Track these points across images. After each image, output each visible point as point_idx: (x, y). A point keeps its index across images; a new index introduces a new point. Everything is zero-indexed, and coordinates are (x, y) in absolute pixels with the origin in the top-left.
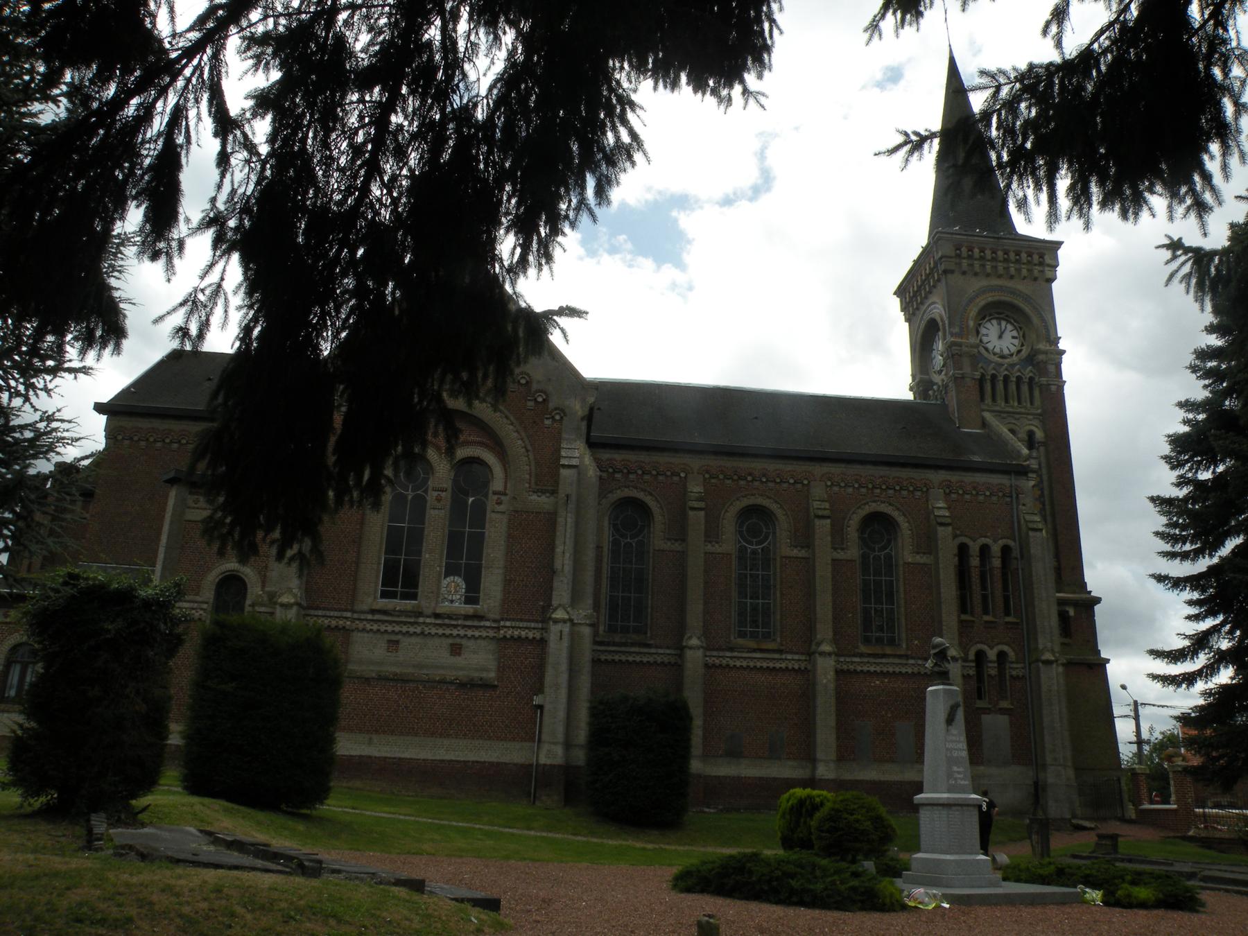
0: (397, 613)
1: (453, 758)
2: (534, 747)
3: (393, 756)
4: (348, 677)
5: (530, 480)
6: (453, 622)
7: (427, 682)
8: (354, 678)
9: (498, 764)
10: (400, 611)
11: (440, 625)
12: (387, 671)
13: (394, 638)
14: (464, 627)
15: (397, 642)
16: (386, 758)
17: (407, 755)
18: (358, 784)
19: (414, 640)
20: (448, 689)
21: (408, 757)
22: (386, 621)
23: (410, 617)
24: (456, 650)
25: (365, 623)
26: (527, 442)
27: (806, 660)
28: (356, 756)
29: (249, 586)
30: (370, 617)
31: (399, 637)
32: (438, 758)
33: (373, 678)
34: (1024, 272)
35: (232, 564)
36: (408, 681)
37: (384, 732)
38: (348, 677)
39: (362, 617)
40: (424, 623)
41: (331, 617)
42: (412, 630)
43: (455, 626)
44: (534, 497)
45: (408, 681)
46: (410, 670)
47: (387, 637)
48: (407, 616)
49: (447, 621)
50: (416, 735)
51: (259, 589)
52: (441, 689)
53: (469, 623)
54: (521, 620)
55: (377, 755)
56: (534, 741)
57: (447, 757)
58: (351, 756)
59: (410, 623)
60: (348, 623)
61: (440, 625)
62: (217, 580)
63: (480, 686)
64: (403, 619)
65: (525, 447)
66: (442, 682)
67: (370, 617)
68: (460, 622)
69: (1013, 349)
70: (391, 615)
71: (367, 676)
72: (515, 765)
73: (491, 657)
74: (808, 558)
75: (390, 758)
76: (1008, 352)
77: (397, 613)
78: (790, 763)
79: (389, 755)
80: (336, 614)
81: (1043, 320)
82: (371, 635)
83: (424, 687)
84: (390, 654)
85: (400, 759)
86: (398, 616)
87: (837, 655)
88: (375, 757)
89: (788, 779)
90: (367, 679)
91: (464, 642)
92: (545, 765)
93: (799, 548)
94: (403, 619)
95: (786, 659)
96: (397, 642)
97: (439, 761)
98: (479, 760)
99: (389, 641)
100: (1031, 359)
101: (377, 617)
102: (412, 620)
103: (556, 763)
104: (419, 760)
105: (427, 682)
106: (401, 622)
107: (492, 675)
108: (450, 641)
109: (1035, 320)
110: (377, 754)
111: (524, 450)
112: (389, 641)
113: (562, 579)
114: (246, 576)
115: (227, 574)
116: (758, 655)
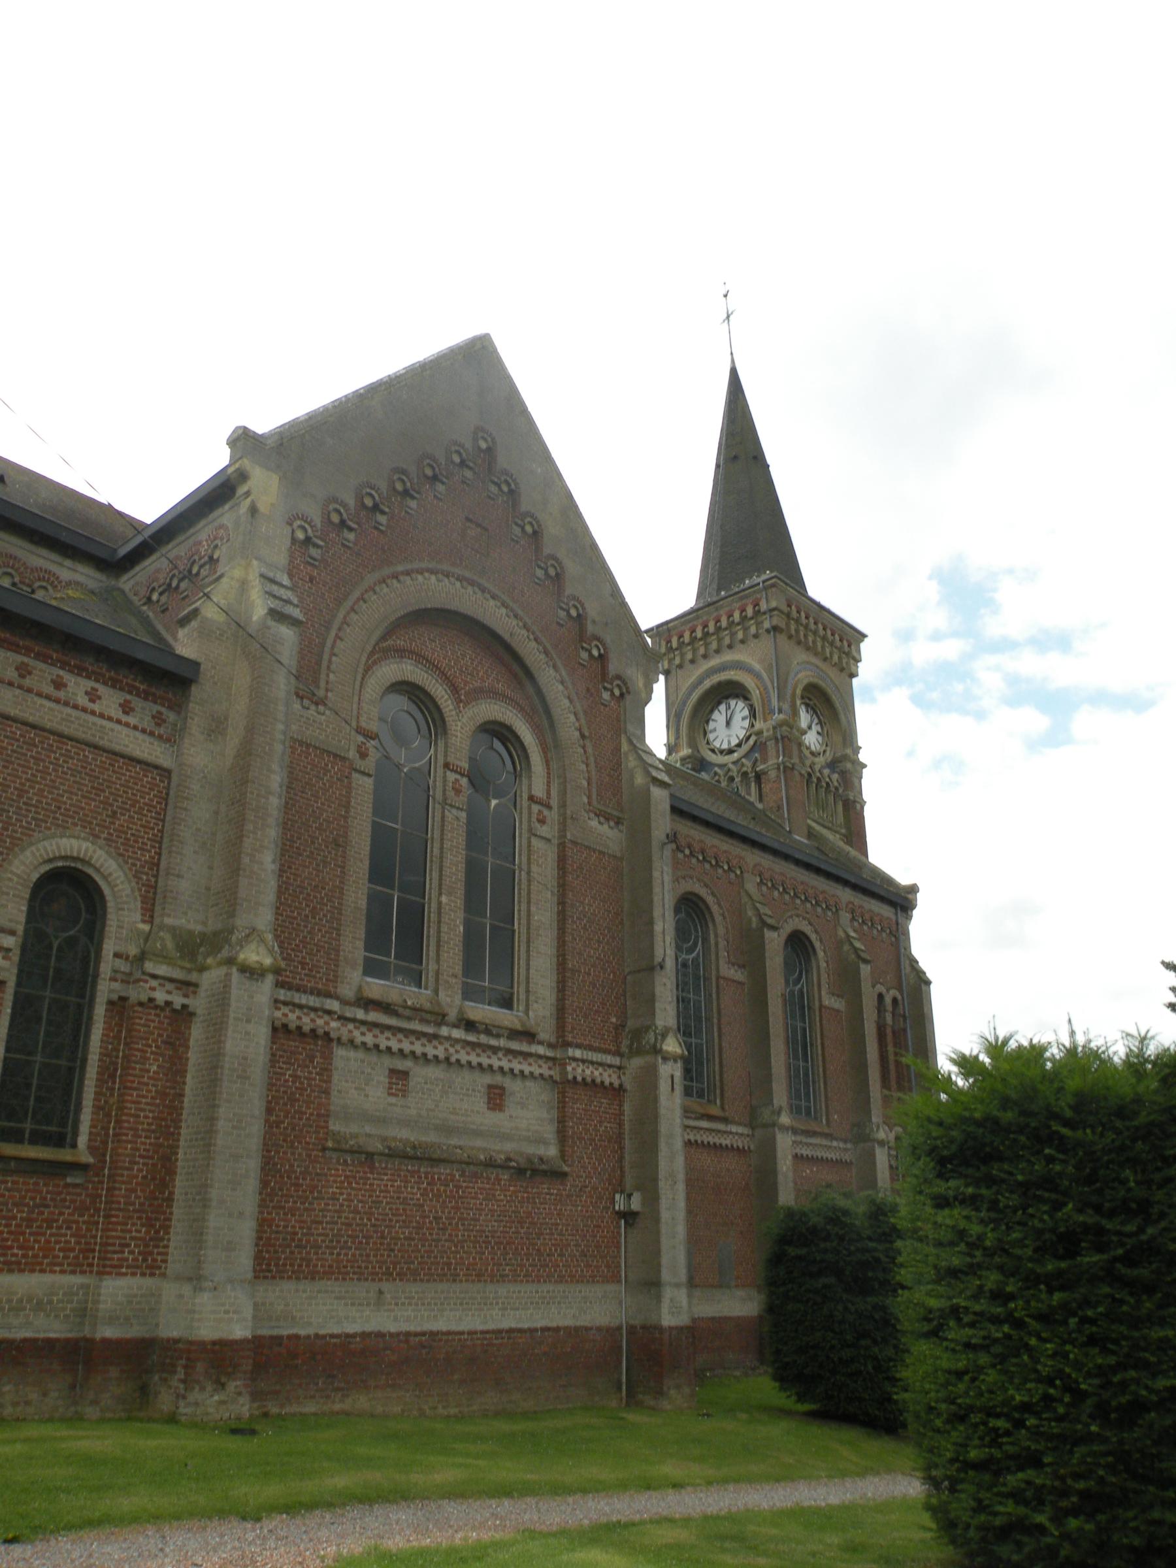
0: (407, 1013)
1: (513, 1325)
2: (620, 1292)
3: (419, 1329)
4: (335, 1150)
5: (590, 791)
6: (493, 1042)
7: (468, 1164)
8: (346, 1151)
9: (577, 1329)
10: (415, 1009)
11: (474, 1045)
12: (395, 1139)
13: (402, 1065)
14: (509, 1052)
15: (405, 1075)
16: (408, 1334)
17: (440, 1325)
18: (361, 1401)
19: (433, 1072)
20: (498, 1180)
21: (444, 1329)
22: (389, 1028)
23: (428, 1022)
24: (496, 1098)
25: (351, 1026)
26: (583, 721)
27: (748, 1136)
28: (354, 1336)
29: (111, 904)
30: (360, 1014)
31: (407, 1064)
32: (491, 1326)
33: (381, 1154)
34: (836, 658)
35: (74, 842)
36: (436, 1161)
37: (401, 1276)
38: (335, 1150)
39: (348, 1015)
40: (448, 1038)
41: (301, 1007)
42: (430, 1051)
43: (495, 1050)
44: (594, 823)
45: (436, 1161)
46: (431, 1138)
47: (388, 1062)
48: (423, 1021)
49: (483, 1039)
50: (455, 1279)
51: (138, 916)
52: (488, 1178)
53: (515, 1045)
54: (590, 1048)
55: (393, 1330)
56: (619, 1281)
57: (506, 1324)
58: (348, 1336)
59: (425, 1035)
60: (334, 1024)
61: (474, 1045)
62: (35, 876)
63: (545, 1173)
64: (416, 1026)
65: (580, 730)
66: (490, 1164)
67: (360, 1014)
68: (502, 1042)
69: (717, 744)
70: (396, 1014)
71: (370, 1149)
72: (599, 1329)
73: (545, 1115)
74: (744, 984)
75: (416, 1334)
76: (711, 739)
77: (407, 1013)
78: (740, 1293)
79: (412, 1328)
80: (313, 1001)
81: (848, 722)
82: (361, 1054)
83: (463, 1174)
84: (393, 1100)
85: (433, 1334)
86: (409, 1019)
87: (774, 1125)
88: (391, 1335)
89: (739, 1318)
90: (370, 1155)
91: (507, 1082)
92: (671, 1328)
93: (736, 967)
94: (416, 1026)
95: (731, 1133)
96: (405, 1075)
97: (493, 1332)
98: (550, 1325)
99: (393, 1072)
100: (833, 765)
101: (374, 1016)
102: (430, 1030)
103: (682, 1324)
104: (462, 1333)
105: (468, 1164)
106: (413, 1032)
107: (552, 1151)
108: (487, 1079)
109: (842, 717)
110: (393, 1328)
111: (577, 734)
112: (393, 1072)
113: (664, 980)
114: (105, 878)
115: (60, 864)
116: (704, 1124)
